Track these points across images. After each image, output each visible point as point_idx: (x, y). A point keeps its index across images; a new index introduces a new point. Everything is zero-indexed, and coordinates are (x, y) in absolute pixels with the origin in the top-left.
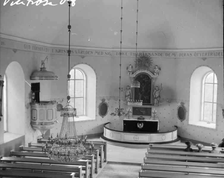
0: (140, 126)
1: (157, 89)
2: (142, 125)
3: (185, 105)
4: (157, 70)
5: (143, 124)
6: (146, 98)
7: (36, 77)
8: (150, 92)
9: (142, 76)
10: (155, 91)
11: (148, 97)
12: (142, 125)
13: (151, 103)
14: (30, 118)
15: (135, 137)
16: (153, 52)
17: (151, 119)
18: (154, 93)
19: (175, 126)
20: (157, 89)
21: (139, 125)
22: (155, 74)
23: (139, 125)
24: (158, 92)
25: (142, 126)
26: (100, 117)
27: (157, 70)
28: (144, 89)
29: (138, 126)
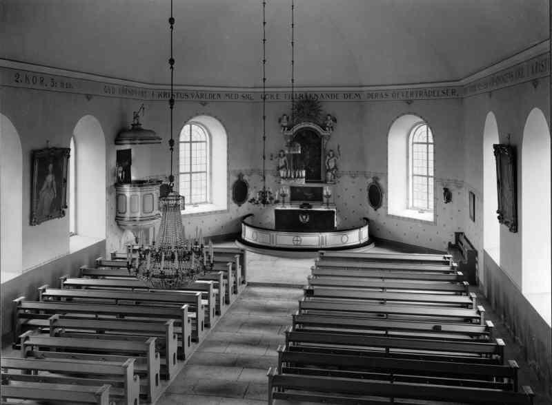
1: (331, 155)
3: (381, 182)
5: (308, 216)
10: (328, 157)
13: (323, 179)
14: (114, 211)
19: (365, 218)
20: (331, 155)
22: (327, 129)
24: (333, 159)
26: (234, 206)
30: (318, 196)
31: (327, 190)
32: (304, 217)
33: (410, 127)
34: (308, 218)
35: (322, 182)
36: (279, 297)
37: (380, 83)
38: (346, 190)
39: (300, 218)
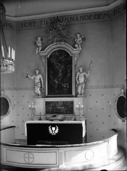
0: (54, 131)
1: (81, 71)
2: (56, 129)
4: (79, 40)
5: (57, 128)
6: (65, 86)
7: (122, 163)
8: (71, 76)
9: (57, 53)
10: (78, 73)
11: (68, 84)
12: (56, 129)
13: (74, 94)
15: (27, 156)
16: (73, 16)
17: (54, 86)
18: (77, 77)
19: (113, 130)
20: (81, 71)
21: (52, 129)
22: (76, 46)
23: (52, 129)
25: (57, 131)
27: (79, 40)
28: (62, 72)
29: (51, 132)
30: (69, 109)
31: (78, 103)
32: (54, 129)
33: (85, 158)
34: (57, 130)
35: (73, 97)
36: (54, 150)
37: (19, 152)
38: (91, 109)
39: (50, 130)
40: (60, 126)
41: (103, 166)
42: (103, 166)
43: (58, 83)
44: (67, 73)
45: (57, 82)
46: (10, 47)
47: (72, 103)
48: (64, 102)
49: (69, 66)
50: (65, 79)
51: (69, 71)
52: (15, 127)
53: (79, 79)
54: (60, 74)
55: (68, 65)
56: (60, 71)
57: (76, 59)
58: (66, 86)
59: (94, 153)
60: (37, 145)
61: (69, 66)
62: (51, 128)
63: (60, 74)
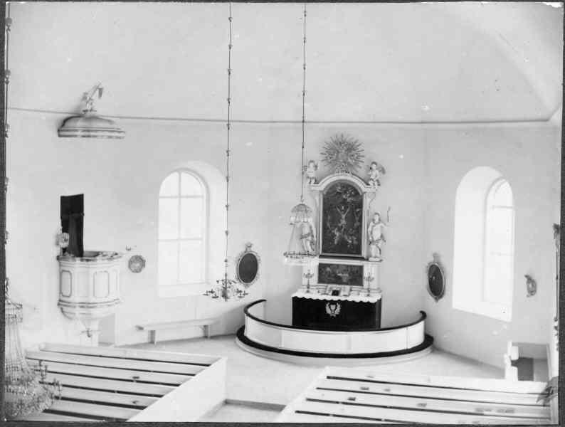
0: (333, 311)
1: (377, 220)
6: (350, 242)
10: (372, 224)
18: (370, 229)
20: (377, 220)
22: (371, 183)
27: (374, 173)
29: (328, 311)
31: (369, 269)
32: (333, 307)
35: (362, 259)
39: (327, 308)
40: (344, 304)
41: (305, 42)
42: (305, 42)
43: (340, 236)
44: (354, 221)
45: (337, 234)
46: (333, 242)
47: (361, 268)
48: (347, 266)
49: (358, 210)
50: (351, 229)
51: (357, 218)
52: (265, 300)
53: (373, 233)
54: (343, 222)
55: (356, 208)
56: (344, 216)
57: (369, 200)
58: (352, 240)
59: (380, 250)
60: (98, 421)
61: (358, 210)
62: (329, 305)
63: (343, 222)
